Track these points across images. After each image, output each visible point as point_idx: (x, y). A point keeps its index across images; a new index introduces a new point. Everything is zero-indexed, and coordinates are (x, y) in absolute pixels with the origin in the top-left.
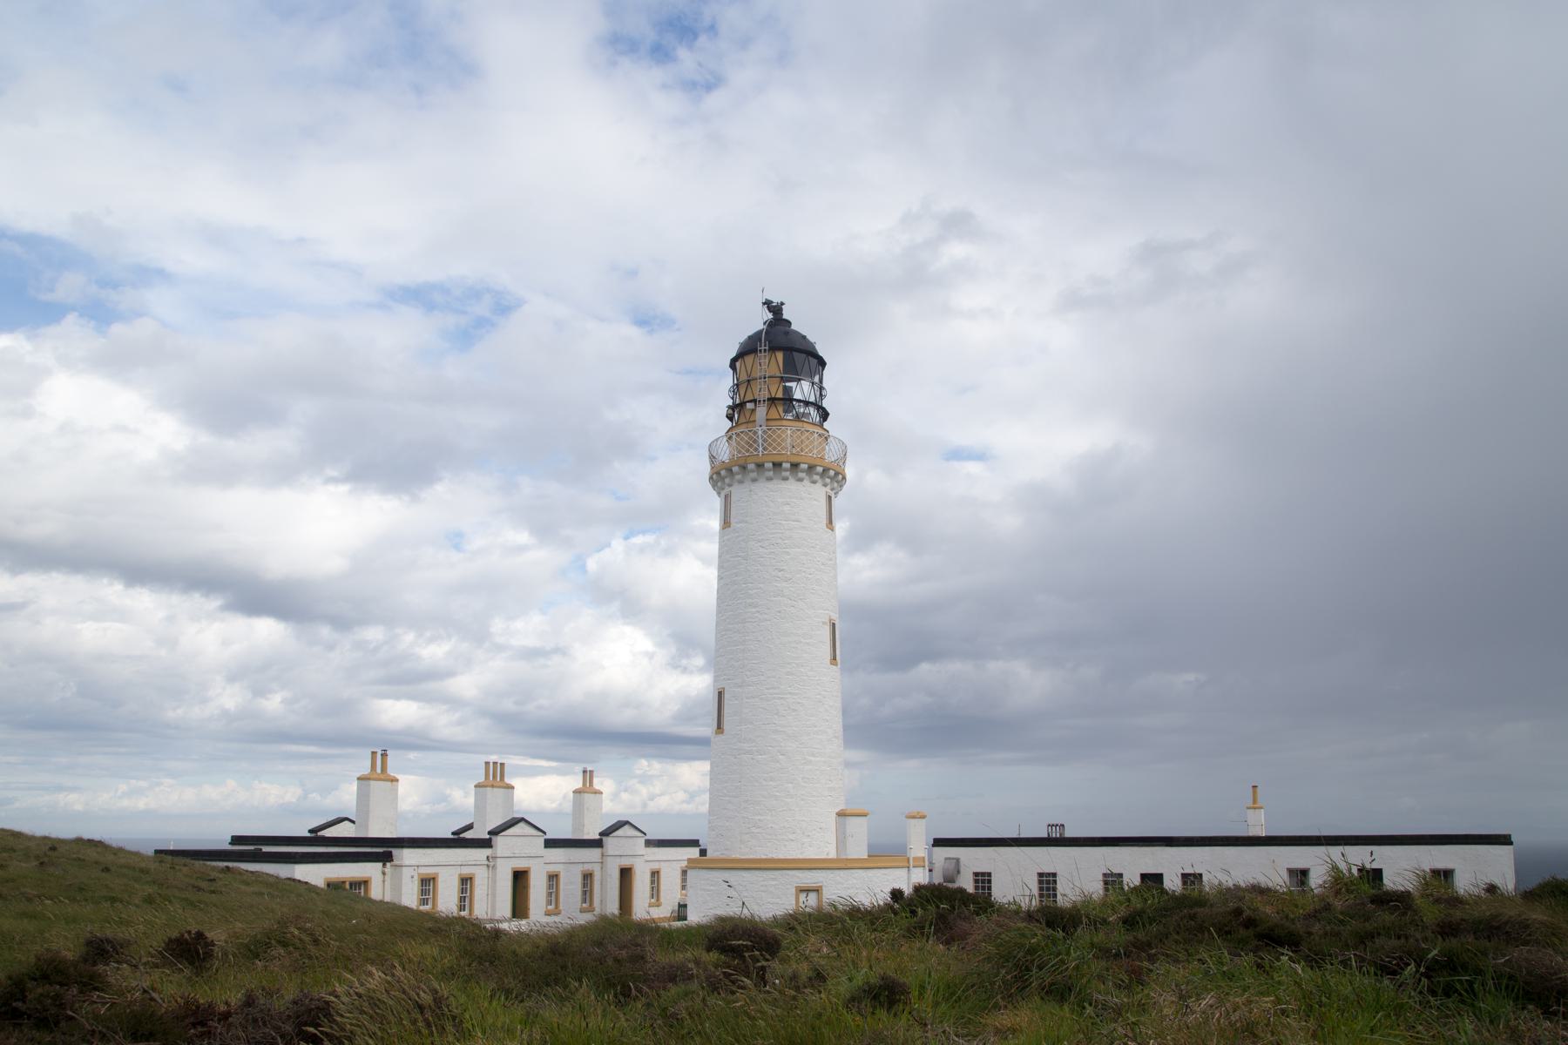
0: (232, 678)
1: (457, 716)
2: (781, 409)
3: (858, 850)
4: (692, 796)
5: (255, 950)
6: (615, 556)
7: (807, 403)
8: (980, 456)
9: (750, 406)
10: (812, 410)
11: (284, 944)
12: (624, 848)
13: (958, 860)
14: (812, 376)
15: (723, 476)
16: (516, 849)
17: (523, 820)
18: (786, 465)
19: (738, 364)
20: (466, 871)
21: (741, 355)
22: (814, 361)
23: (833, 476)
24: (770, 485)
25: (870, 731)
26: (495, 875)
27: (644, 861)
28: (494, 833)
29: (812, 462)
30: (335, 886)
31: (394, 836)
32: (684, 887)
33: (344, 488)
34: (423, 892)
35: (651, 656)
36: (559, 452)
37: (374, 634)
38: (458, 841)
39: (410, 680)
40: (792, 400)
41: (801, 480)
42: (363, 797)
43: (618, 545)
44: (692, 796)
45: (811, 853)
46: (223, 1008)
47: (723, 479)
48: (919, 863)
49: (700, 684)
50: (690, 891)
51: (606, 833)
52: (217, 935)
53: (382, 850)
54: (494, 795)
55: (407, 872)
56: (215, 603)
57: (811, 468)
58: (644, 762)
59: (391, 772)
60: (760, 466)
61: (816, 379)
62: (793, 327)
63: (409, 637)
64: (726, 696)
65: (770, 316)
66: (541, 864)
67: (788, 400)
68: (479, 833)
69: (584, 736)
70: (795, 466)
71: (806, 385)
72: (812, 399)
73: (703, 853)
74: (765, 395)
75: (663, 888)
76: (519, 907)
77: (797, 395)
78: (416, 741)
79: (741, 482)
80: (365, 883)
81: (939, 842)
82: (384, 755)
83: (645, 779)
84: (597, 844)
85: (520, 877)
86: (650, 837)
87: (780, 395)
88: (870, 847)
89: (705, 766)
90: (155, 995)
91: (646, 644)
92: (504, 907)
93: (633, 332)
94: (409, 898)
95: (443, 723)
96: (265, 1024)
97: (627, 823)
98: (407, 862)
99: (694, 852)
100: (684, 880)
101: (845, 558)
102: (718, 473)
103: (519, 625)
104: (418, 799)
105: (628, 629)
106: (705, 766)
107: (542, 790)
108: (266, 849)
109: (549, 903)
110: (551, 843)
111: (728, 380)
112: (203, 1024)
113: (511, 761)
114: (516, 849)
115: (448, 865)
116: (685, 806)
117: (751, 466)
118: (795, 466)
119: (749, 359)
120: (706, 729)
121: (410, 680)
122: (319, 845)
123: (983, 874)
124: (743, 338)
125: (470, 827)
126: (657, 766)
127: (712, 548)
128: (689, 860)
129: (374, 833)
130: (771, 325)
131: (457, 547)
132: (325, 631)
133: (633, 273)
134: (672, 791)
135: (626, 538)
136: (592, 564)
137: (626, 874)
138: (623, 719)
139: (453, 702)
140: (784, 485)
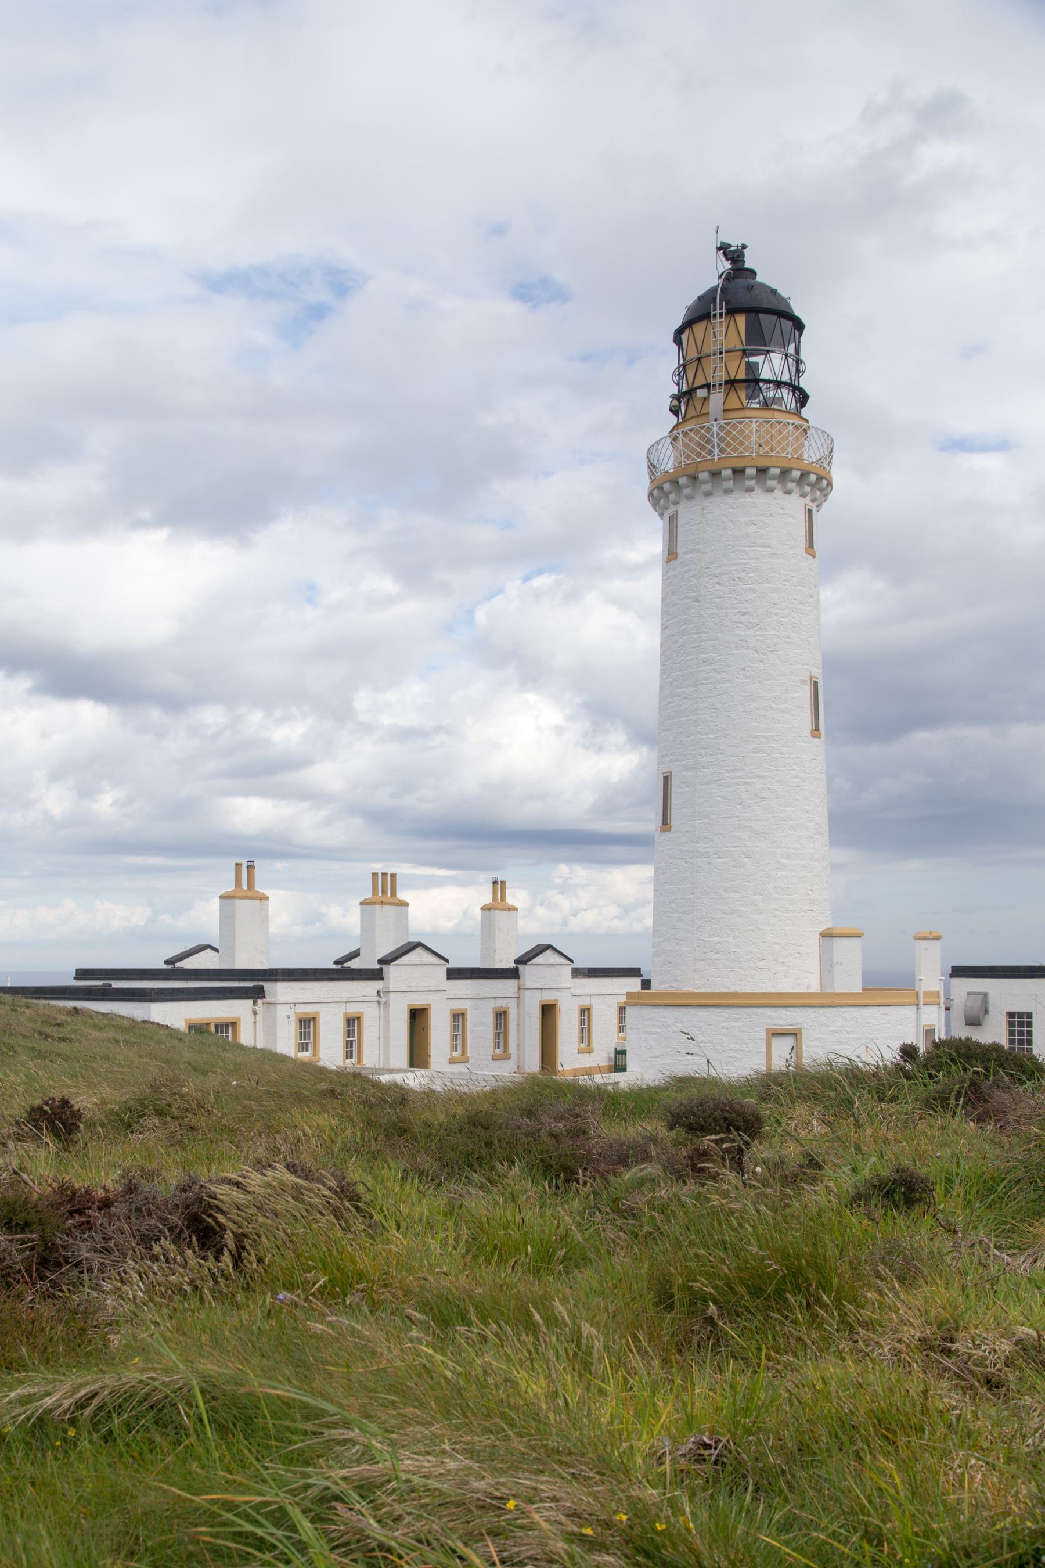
0: (57, 775)
1: (322, 814)
2: (743, 395)
3: (849, 982)
4: (626, 909)
5: (125, 1121)
6: (515, 604)
7: (779, 384)
8: (1001, 446)
9: (701, 393)
10: (786, 394)
11: (160, 1113)
12: (547, 979)
13: (985, 996)
14: (785, 345)
15: (667, 490)
16: (414, 981)
17: (420, 945)
18: (751, 471)
19: (684, 337)
20: (353, 1009)
21: (688, 324)
22: (787, 325)
23: (815, 482)
24: (729, 499)
25: (858, 826)
26: (387, 1012)
27: (571, 995)
28: (385, 961)
29: (785, 464)
30: (198, 1029)
31: (266, 967)
32: (621, 1029)
33: (162, 534)
34: (302, 1035)
35: (559, 731)
36: (427, 472)
37: (213, 716)
38: (342, 972)
39: (264, 772)
40: (757, 381)
41: (770, 490)
42: (227, 919)
43: (513, 587)
44: (626, 909)
45: (785, 986)
46: (100, 1193)
47: (666, 495)
48: (932, 999)
49: (623, 763)
50: (630, 1034)
51: (522, 961)
52: (84, 1101)
53: (251, 984)
54: (384, 914)
55: (282, 1012)
56: (24, 683)
57: (785, 473)
58: (564, 869)
59: (259, 888)
60: (715, 474)
61: (791, 349)
62: (759, 279)
63: (256, 717)
64: (674, 782)
65: (728, 265)
66: (443, 1000)
67: (753, 382)
68: (367, 961)
69: (484, 835)
70: (762, 471)
71: (776, 358)
72: (786, 378)
73: (646, 984)
74: (721, 376)
75: (595, 1028)
76: (418, 1056)
77: (765, 374)
78: (280, 847)
79: (690, 498)
80: (234, 1024)
81: (958, 972)
82: (251, 867)
83: (567, 888)
84: (512, 974)
85: (417, 1016)
86: (577, 964)
87: (742, 375)
88: (866, 976)
89: (647, 872)
90: (25, 1177)
91: (553, 715)
92: (400, 1055)
93: (512, 309)
94: (286, 1044)
95: (307, 823)
96: (150, 1214)
97: (549, 947)
98: (281, 999)
99: (633, 984)
100: (622, 1020)
101: (824, 598)
102: (660, 488)
103: (391, 696)
104: (298, 919)
105: (531, 697)
106: (647, 872)
107: (442, 906)
108: (117, 984)
109: (454, 1048)
110: (454, 974)
111: (671, 359)
112: (80, 1212)
113: (403, 870)
114: (414, 981)
115: (331, 1002)
116: (616, 923)
117: (704, 476)
118: (762, 471)
119: (699, 328)
120: (650, 822)
121: (264, 772)
122: (176, 979)
123: (1021, 1015)
124: (691, 299)
125: (355, 954)
126: (580, 873)
127: (650, 587)
128: (629, 995)
129: (243, 962)
130: (728, 278)
131: (311, 601)
132: (155, 714)
133: (499, 230)
134: (601, 905)
135: (527, 579)
136: (481, 616)
137: (548, 1011)
138: (526, 813)
139: (313, 796)
140: (748, 499)
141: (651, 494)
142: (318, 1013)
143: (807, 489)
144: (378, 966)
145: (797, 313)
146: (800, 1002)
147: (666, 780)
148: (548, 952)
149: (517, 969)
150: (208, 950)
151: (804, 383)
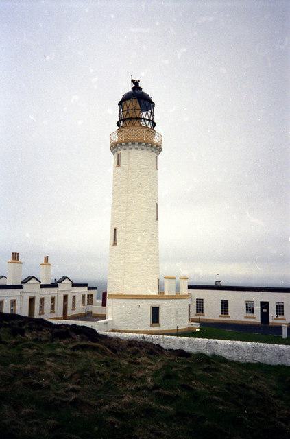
12: (65, 288)
15: (114, 147)
16: (31, 289)
22: (147, 103)
84: (19, 287)
97: (33, 277)
110: (42, 286)
119: (128, 102)
137: (65, 297)
142: (220, 316)
147: (115, 230)
148: (33, 279)
149: (21, 286)
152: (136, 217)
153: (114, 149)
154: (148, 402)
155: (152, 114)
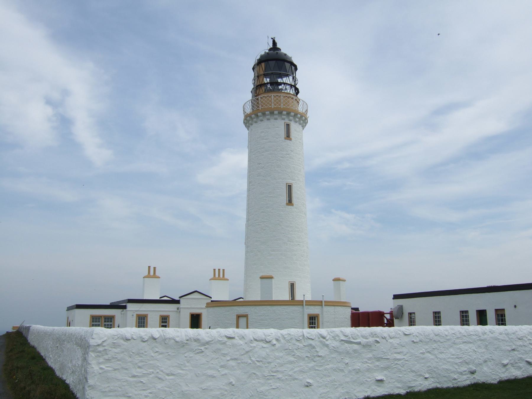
55: (129, 314)
141: (244, 122)
143: (302, 122)
144: (179, 299)
145: (295, 63)
146: (339, 304)
147: (290, 202)
150: (196, 296)
151: (297, 86)
152: (272, 197)
153: (249, 121)
154: (378, 389)
155: (294, 79)
